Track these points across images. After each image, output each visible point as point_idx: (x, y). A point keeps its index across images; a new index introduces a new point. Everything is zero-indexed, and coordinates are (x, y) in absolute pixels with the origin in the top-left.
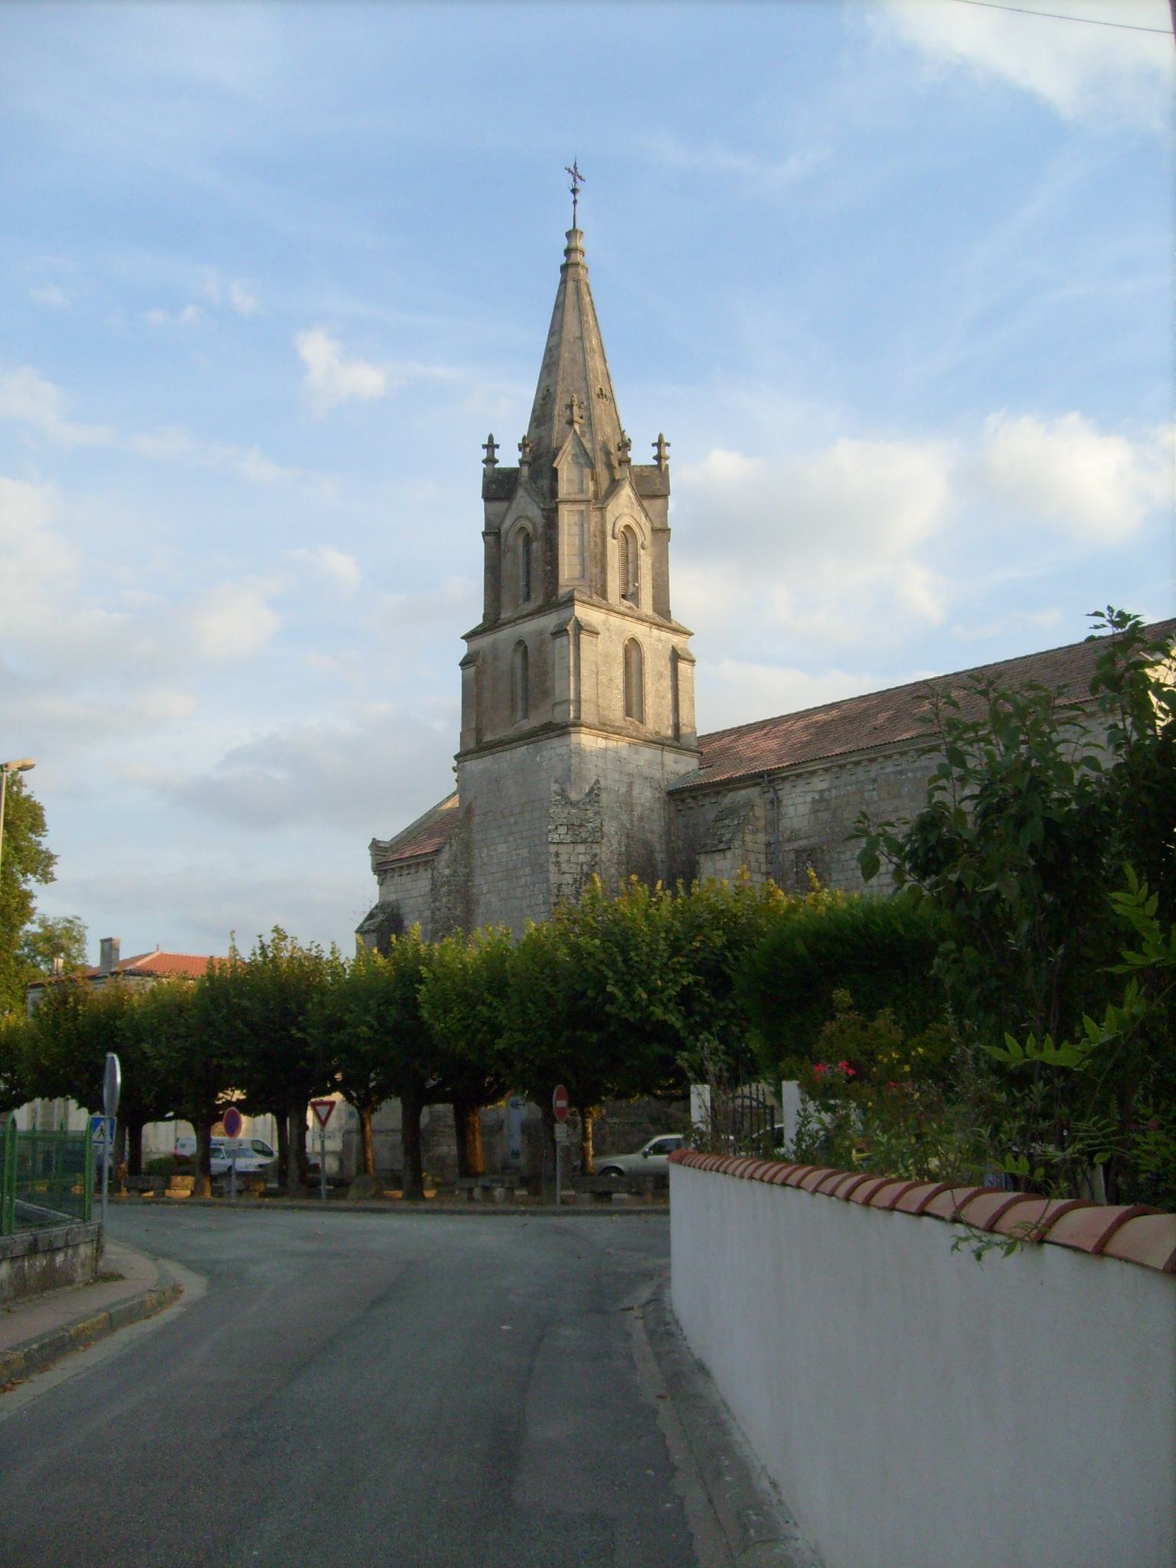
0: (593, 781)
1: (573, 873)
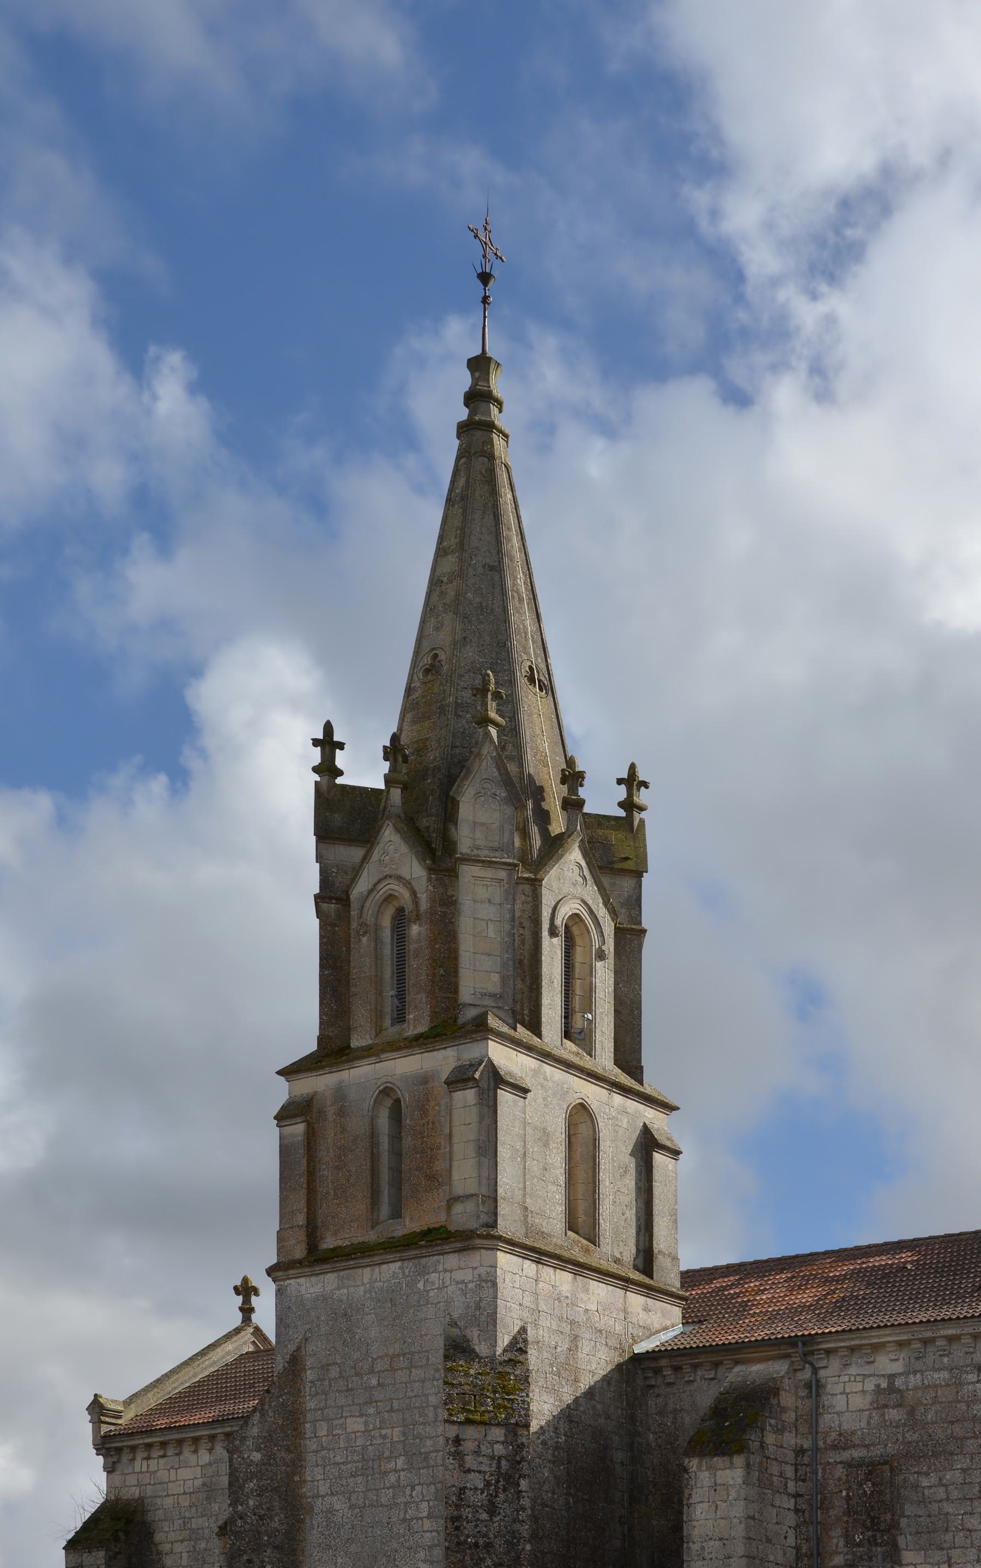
0: (517, 1329)
1: (485, 1472)
